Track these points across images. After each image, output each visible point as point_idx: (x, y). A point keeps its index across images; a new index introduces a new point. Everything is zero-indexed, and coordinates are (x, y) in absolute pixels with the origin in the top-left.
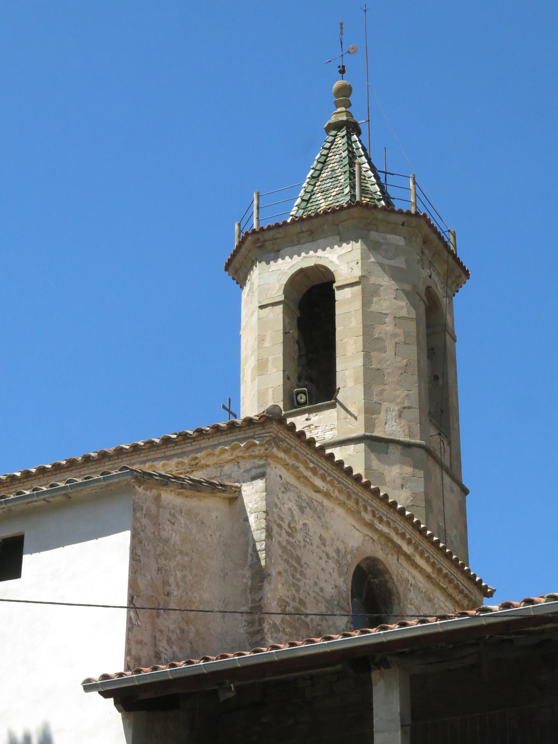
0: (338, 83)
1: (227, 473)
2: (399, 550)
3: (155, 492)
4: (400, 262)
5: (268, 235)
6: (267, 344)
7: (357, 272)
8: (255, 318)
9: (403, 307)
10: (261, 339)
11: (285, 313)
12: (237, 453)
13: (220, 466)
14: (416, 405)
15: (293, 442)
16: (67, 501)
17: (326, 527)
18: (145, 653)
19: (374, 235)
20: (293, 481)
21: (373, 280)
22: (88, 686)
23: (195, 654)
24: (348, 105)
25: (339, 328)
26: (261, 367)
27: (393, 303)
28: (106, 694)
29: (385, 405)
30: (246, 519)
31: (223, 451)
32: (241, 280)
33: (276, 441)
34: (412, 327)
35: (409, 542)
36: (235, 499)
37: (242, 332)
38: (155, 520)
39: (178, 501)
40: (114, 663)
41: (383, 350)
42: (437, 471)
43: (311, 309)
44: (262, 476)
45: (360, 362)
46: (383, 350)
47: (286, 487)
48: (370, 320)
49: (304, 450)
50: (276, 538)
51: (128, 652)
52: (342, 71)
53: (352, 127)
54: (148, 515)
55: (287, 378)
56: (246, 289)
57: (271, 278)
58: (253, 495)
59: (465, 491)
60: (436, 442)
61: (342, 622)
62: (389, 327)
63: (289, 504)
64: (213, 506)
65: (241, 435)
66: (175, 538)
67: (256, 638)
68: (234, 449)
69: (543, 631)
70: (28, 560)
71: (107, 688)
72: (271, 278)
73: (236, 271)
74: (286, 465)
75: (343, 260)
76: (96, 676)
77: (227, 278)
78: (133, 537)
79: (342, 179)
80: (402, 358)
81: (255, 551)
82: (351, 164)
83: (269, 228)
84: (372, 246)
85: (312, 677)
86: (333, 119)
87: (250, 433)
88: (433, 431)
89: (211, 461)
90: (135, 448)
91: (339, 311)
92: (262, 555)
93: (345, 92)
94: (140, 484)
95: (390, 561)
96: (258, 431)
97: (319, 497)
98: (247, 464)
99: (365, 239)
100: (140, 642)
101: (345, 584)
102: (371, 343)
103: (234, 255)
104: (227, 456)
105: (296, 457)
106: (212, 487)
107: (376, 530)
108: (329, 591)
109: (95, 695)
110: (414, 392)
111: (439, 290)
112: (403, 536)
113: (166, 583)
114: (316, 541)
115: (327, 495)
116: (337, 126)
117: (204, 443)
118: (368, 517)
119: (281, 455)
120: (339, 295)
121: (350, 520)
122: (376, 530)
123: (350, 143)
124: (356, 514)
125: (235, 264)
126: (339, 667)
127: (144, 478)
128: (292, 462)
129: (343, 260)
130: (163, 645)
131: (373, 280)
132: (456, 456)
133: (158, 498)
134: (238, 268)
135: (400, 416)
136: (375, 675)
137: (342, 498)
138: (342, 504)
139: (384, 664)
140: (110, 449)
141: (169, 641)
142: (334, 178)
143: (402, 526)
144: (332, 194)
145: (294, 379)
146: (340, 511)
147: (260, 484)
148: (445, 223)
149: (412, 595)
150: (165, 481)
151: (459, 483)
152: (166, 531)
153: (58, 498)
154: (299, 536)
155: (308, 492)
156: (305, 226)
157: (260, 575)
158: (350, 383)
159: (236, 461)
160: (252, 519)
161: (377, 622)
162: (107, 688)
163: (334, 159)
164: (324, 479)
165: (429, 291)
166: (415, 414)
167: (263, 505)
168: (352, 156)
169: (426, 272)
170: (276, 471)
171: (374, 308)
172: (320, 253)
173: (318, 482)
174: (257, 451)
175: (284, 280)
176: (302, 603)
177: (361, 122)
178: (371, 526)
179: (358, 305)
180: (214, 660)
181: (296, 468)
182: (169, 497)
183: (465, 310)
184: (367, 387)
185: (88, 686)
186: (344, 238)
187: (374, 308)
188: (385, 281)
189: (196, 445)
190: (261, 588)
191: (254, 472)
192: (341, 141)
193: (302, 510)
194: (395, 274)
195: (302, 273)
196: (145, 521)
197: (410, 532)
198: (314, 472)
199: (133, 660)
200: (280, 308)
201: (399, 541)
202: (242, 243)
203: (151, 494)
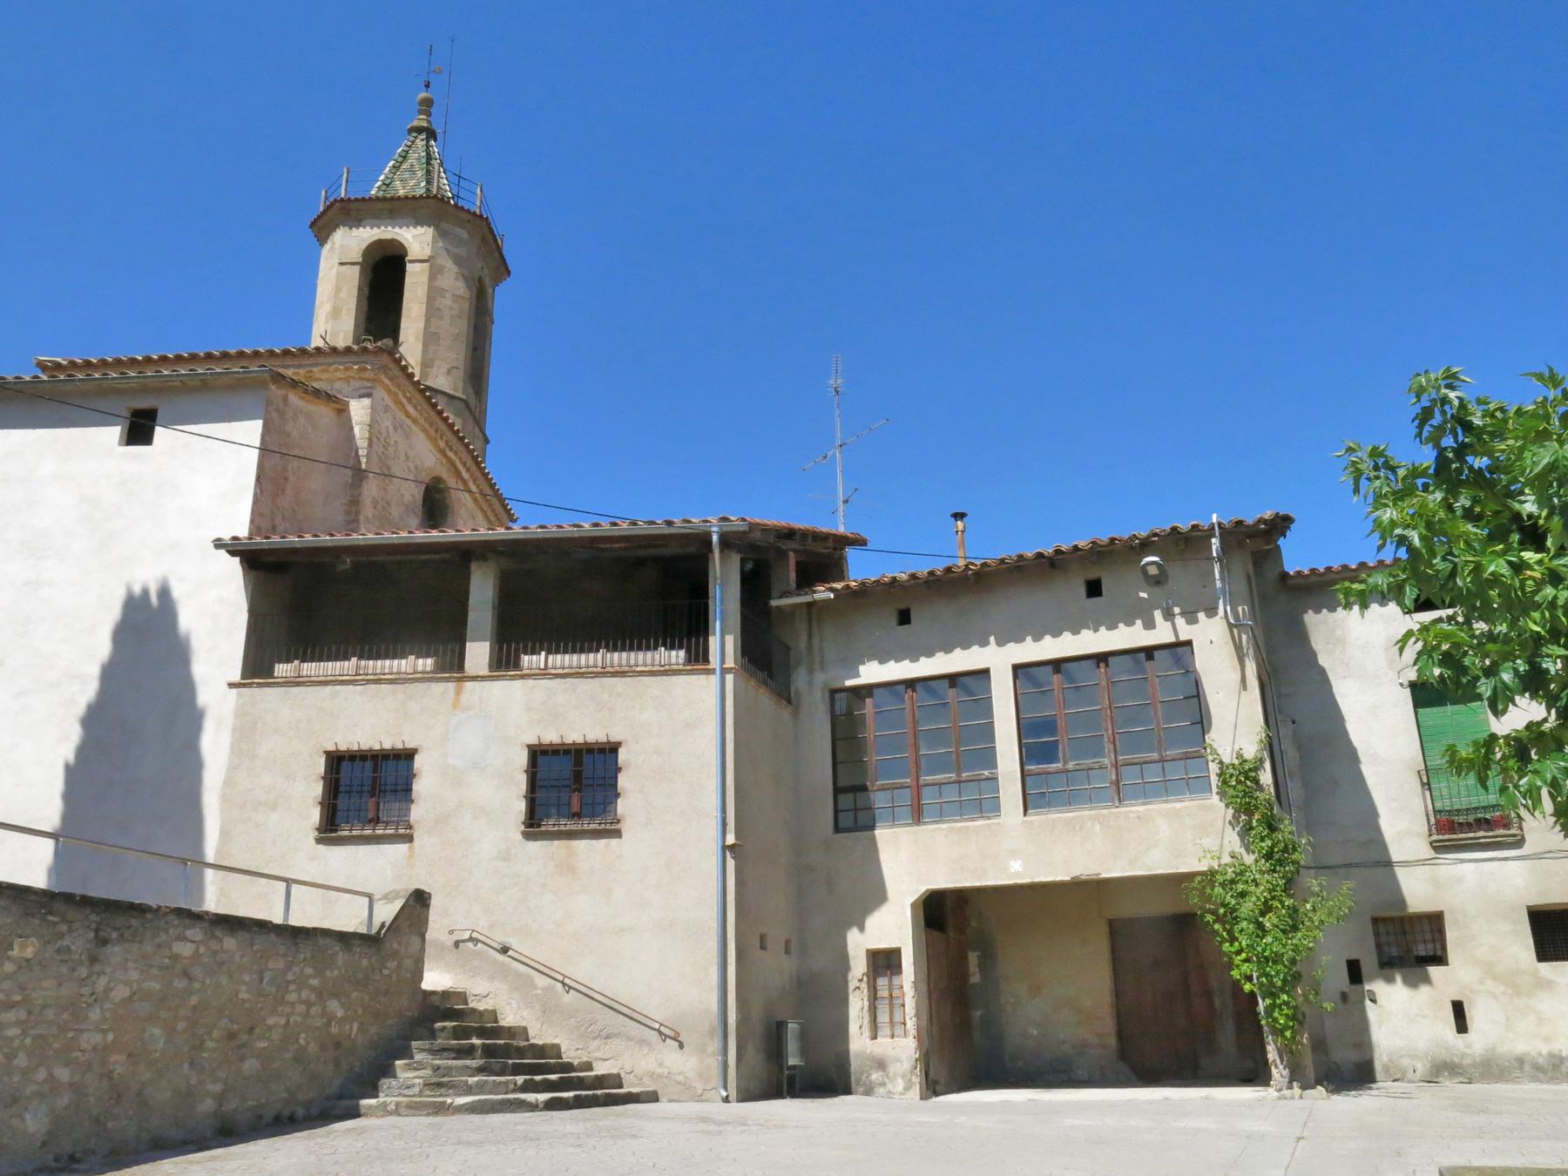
0: (423, 95)
1: (338, 389)
2: (458, 474)
3: (283, 392)
4: (462, 251)
5: (352, 205)
6: (343, 295)
7: (427, 252)
8: (334, 271)
9: (461, 288)
10: (338, 290)
11: (362, 272)
12: (350, 373)
13: (331, 381)
14: (461, 366)
15: (397, 372)
16: (204, 386)
17: (411, 447)
18: (265, 524)
19: (444, 225)
20: (392, 405)
21: (439, 261)
22: (219, 544)
23: (274, 529)
24: (429, 114)
25: (406, 294)
26: (335, 313)
27: (453, 283)
28: (232, 553)
29: (437, 362)
30: (352, 429)
31: (336, 370)
32: (322, 239)
33: (385, 369)
34: (466, 305)
35: (468, 470)
36: (343, 411)
37: (319, 282)
38: (282, 414)
39: (301, 403)
40: (243, 531)
41: (441, 318)
42: (471, 422)
43: (384, 276)
44: (368, 395)
45: (422, 325)
46: (441, 318)
47: (387, 409)
48: (433, 293)
49: (403, 380)
50: (375, 447)
51: (252, 521)
52: (427, 86)
53: (431, 134)
54: (277, 410)
55: (356, 326)
56: (327, 247)
57: (351, 242)
58: (359, 410)
59: (487, 441)
60: (473, 402)
61: (414, 521)
62: (448, 301)
63: (386, 423)
64: (324, 412)
65: (354, 359)
66: (295, 434)
67: (352, 524)
68: (347, 369)
69: (611, 549)
70: (159, 431)
71: (233, 548)
72: (351, 242)
73: (320, 230)
74: (388, 391)
75: (416, 239)
76: (226, 536)
77: (310, 234)
78: (265, 426)
79: (419, 173)
80: (455, 327)
81: (357, 456)
82: (428, 163)
83: (356, 200)
84: (442, 234)
85: (399, 563)
86: (415, 123)
87: (364, 358)
88: (471, 390)
89: (324, 376)
90: (286, 353)
91: (408, 280)
92: (363, 460)
93: (427, 104)
94: (275, 382)
95: (451, 482)
96: (371, 358)
97: (408, 422)
98: (355, 384)
99: (437, 227)
100: (261, 515)
101: (419, 497)
102: (432, 312)
103: (319, 217)
104: (339, 374)
105: (398, 387)
106: (329, 398)
107: (446, 456)
108: (408, 498)
109: (223, 552)
110: (462, 357)
111: (487, 281)
112: (464, 464)
113: (285, 470)
114: (403, 457)
115: (415, 421)
116: (419, 130)
117: (321, 360)
118: (442, 444)
119: (387, 381)
120: (409, 267)
121: (428, 444)
122: (446, 456)
123: (428, 146)
124: (433, 440)
125: (320, 223)
126: (446, 556)
127: (278, 378)
128: (394, 389)
129: (416, 239)
130: (278, 520)
131: (439, 261)
132: (483, 412)
133: (285, 398)
134: (322, 228)
135: (449, 372)
136: (474, 566)
137: (426, 426)
138: (425, 431)
139: (483, 557)
140: (233, 351)
141: (283, 518)
142: (412, 170)
143: (465, 455)
144: (410, 184)
145: (362, 327)
146: (422, 435)
147: (366, 402)
148: (499, 227)
149: (463, 512)
150: (294, 384)
151: (483, 432)
152: (289, 427)
153: (196, 383)
154: (391, 449)
155: (401, 416)
156: (387, 205)
157: (359, 475)
158: (412, 339)
159: (347, 380)
160: (357, 430)
161: (433, 527)
162: (233, 548)
163: (413, 157)
164: (415, 407)
165: (480, 280)
166: (460, 373)
167: (367, 419)
168: (429, 157)
169: (479, 265)
170: (380, 393)
171: (438, 283)
172: (397, 230)
173: (410, 409)
174: (367, 375)
175: (364, 246)
176: (388, 503)
177: (439, 131)
178: (443, 452)
179: (425, 278)
180: (308, 537)
181: (396, 395)
182: (294, 398)
183: (503, 297)
184: (425, 345)
185: (219, 544)
186: (419, 222)
187: (438, 283)
188: (449, 264)
189: (312, 361)
190: (360, 486)
191: (362, 391)
192: (420, 143)
193: (395, 429)
194: (458, 261)
195: (379, 244)
196: (274, 415)
197: (470, 463)
198: (409, 400)
199: (255, 527)
200: (357, 268)
201: (460, 467)
202: (328, 208)
203: (280, 393)
